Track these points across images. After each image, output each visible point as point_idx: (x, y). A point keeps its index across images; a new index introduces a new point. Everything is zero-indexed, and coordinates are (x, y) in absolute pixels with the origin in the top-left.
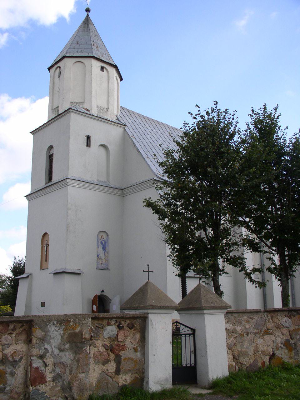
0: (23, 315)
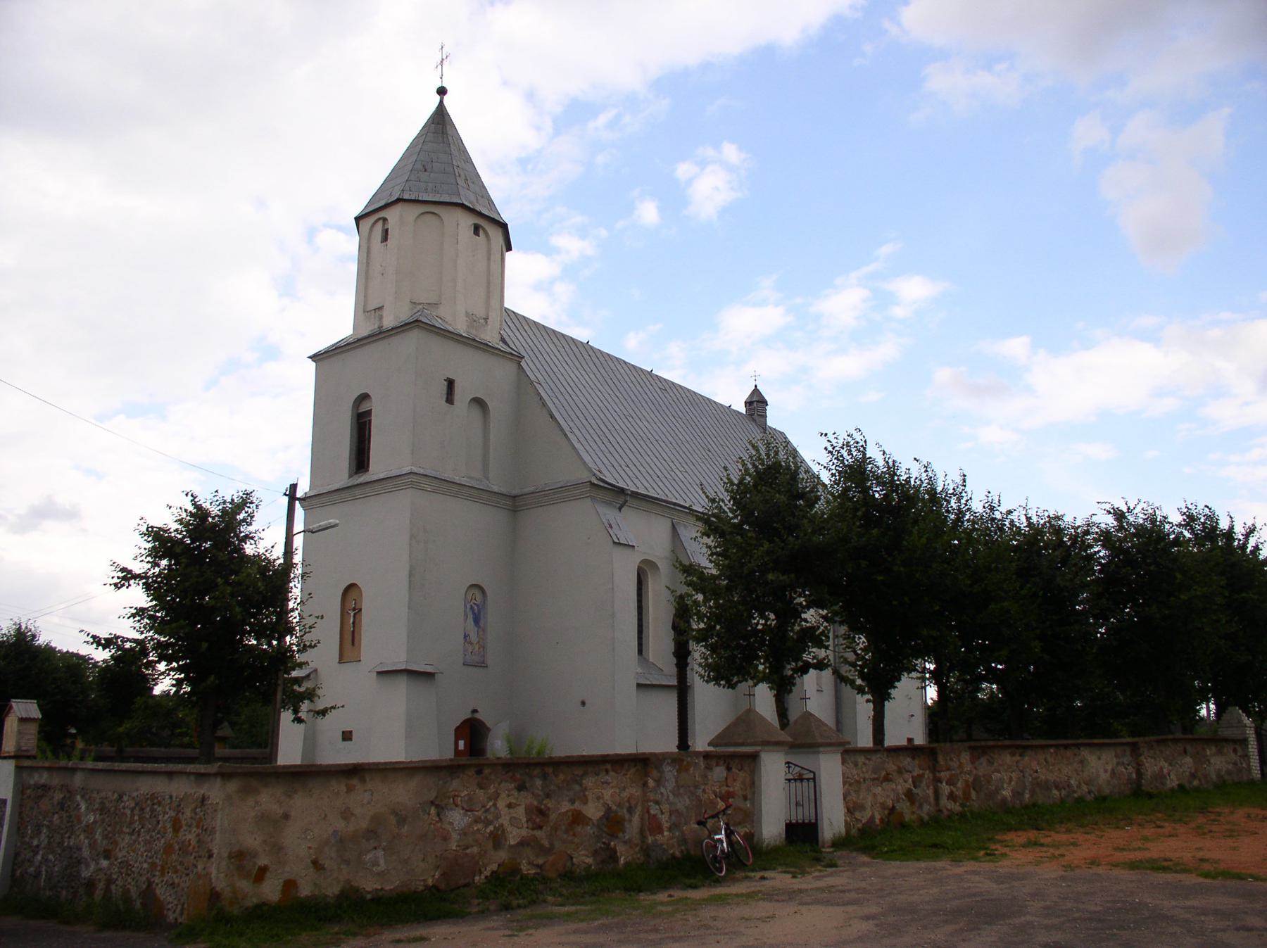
0: (299, 762)
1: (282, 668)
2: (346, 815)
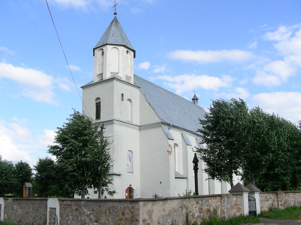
1: (237, 179)
2: (164, 210)
